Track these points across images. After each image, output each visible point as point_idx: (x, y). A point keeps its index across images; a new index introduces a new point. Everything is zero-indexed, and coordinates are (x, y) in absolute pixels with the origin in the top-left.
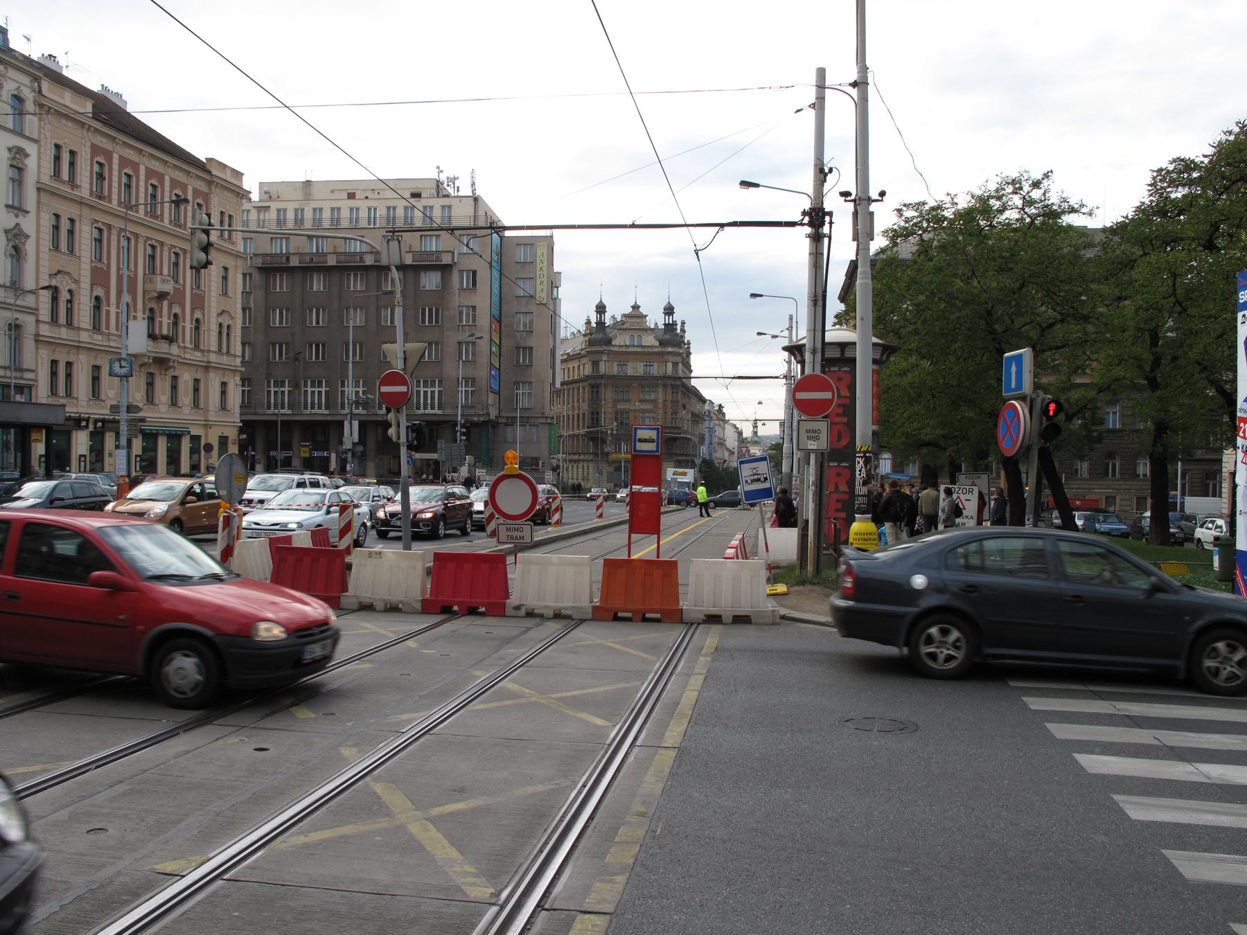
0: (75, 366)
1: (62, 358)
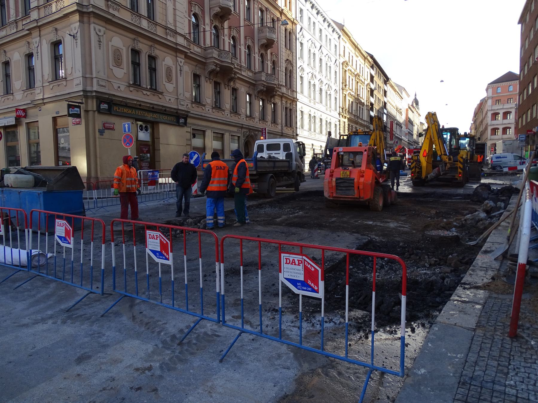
0: (159, 62)
1: (143, 47)
